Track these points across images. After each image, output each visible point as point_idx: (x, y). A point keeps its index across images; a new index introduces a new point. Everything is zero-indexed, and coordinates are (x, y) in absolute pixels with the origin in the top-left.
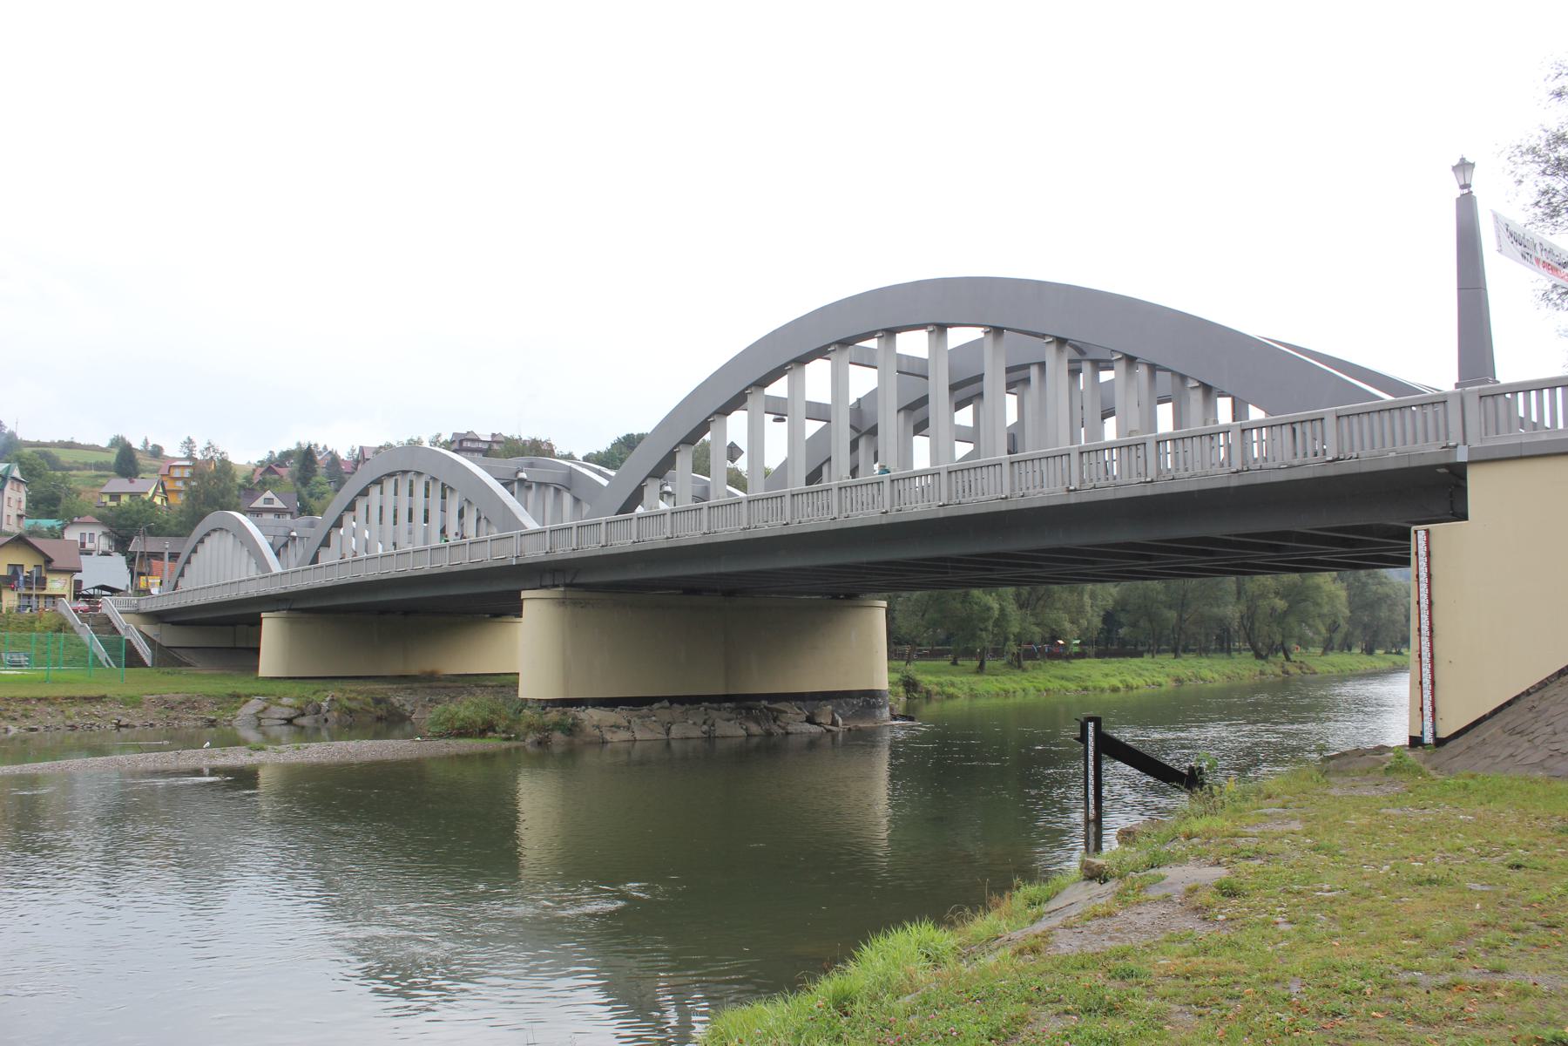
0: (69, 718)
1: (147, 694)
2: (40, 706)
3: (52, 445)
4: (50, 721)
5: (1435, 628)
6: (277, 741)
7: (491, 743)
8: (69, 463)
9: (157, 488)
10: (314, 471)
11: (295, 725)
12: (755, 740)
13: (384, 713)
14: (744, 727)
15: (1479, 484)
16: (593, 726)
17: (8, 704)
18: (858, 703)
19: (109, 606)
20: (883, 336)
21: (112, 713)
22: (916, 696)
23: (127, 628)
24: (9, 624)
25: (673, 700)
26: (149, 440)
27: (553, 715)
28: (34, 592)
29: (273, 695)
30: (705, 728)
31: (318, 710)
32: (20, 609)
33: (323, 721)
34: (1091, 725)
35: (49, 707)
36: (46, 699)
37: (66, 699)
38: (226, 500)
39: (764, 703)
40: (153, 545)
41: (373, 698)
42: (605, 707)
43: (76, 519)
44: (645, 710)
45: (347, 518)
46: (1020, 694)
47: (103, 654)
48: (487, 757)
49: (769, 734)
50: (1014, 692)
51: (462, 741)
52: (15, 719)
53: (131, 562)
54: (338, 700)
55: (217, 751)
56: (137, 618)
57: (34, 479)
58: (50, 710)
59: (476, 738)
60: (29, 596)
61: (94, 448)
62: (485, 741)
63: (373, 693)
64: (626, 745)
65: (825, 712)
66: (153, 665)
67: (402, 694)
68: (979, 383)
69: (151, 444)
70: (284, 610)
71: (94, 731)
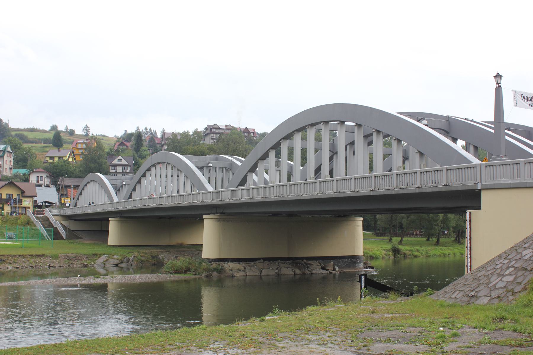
0: (31, 263)
1: (61, 254)
2: (20, 258)
3: (24, 130)
4: (24, 264)
5: (472, 247)
6: (112, 273)
7: (188, 276)
8: (32, 139)
9: (70, 154)
10: (142, 145)
11: (119, 267)
12: (297, 277)
13: (155, 262)
14: (294, 271)
15: (485, 196)
16: (229, 270)
17: (8, 257)
18: (348, 261)
19: (48, 212)
20: (323, 124)
21: (47, 261)
22: (399, 256)
23: (55, 222)
24: (7, 221)
25: (265, 259)
26: (68, 127)
27: (214, 265)
28: (17, 206)
29: (111, 254)
30: (277, 271)
31: (128, 261)
32: (11, 213)
33: (130, 265)
34: (363, 277)
35: (23, 259)
36: (22, 255)
37: (30, 255)
38: (101, 161)
39: (305, 261)
40: (68, 181)
41: (151, 256)
42: (236, 262)
43: (35, 170)
44: (252, 263)
45: (147, 174)
46: (452, 256)
47: (45, 234)
48: (187, 281)
49: (304, 274)
50: (449, 255)
51: (176, 275)
52: (11, 263)
53: (58, 190)
54: (137, 257)
55: (82, 278)
56: (59, 218)
57: (17, 150)
58: (24, 260)
59: (183, 274)
60: (15, 208)
61: (44, 131)
62: (186, 275)
63: (152, 253)
64: (243, 277)
65: (330, 266)
66: (66, 239)
67: (164, 254)
68: (372, 136)
69: (69, 129)
70: (118, 217)
71: (40, 268)
